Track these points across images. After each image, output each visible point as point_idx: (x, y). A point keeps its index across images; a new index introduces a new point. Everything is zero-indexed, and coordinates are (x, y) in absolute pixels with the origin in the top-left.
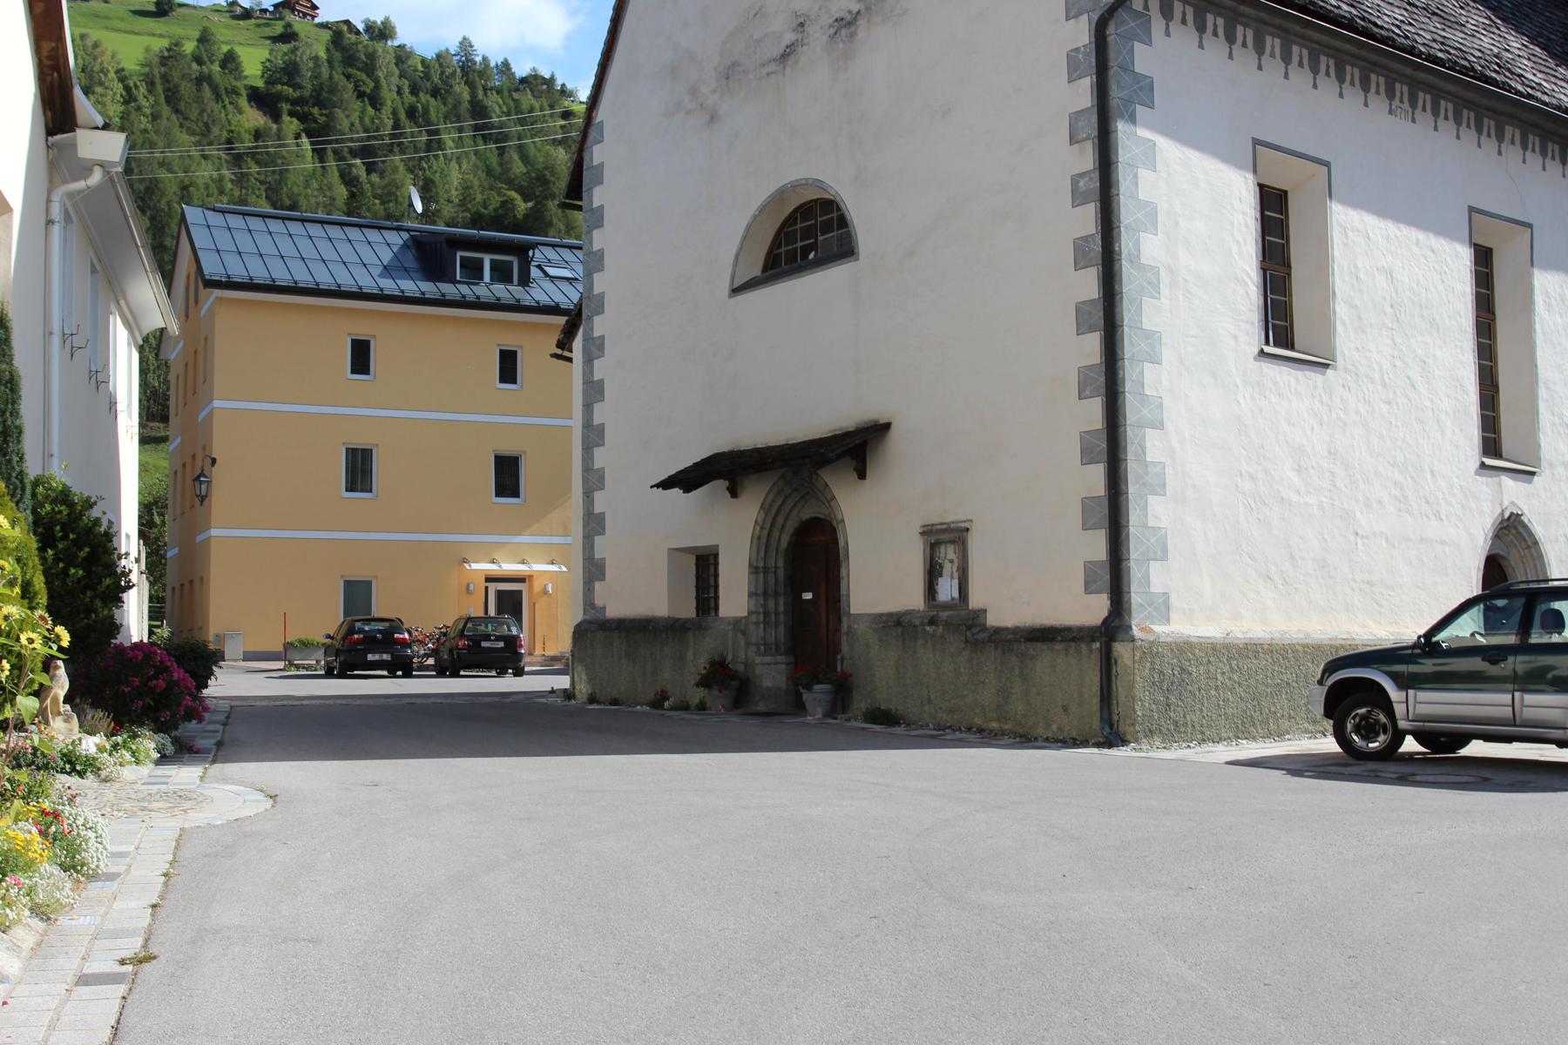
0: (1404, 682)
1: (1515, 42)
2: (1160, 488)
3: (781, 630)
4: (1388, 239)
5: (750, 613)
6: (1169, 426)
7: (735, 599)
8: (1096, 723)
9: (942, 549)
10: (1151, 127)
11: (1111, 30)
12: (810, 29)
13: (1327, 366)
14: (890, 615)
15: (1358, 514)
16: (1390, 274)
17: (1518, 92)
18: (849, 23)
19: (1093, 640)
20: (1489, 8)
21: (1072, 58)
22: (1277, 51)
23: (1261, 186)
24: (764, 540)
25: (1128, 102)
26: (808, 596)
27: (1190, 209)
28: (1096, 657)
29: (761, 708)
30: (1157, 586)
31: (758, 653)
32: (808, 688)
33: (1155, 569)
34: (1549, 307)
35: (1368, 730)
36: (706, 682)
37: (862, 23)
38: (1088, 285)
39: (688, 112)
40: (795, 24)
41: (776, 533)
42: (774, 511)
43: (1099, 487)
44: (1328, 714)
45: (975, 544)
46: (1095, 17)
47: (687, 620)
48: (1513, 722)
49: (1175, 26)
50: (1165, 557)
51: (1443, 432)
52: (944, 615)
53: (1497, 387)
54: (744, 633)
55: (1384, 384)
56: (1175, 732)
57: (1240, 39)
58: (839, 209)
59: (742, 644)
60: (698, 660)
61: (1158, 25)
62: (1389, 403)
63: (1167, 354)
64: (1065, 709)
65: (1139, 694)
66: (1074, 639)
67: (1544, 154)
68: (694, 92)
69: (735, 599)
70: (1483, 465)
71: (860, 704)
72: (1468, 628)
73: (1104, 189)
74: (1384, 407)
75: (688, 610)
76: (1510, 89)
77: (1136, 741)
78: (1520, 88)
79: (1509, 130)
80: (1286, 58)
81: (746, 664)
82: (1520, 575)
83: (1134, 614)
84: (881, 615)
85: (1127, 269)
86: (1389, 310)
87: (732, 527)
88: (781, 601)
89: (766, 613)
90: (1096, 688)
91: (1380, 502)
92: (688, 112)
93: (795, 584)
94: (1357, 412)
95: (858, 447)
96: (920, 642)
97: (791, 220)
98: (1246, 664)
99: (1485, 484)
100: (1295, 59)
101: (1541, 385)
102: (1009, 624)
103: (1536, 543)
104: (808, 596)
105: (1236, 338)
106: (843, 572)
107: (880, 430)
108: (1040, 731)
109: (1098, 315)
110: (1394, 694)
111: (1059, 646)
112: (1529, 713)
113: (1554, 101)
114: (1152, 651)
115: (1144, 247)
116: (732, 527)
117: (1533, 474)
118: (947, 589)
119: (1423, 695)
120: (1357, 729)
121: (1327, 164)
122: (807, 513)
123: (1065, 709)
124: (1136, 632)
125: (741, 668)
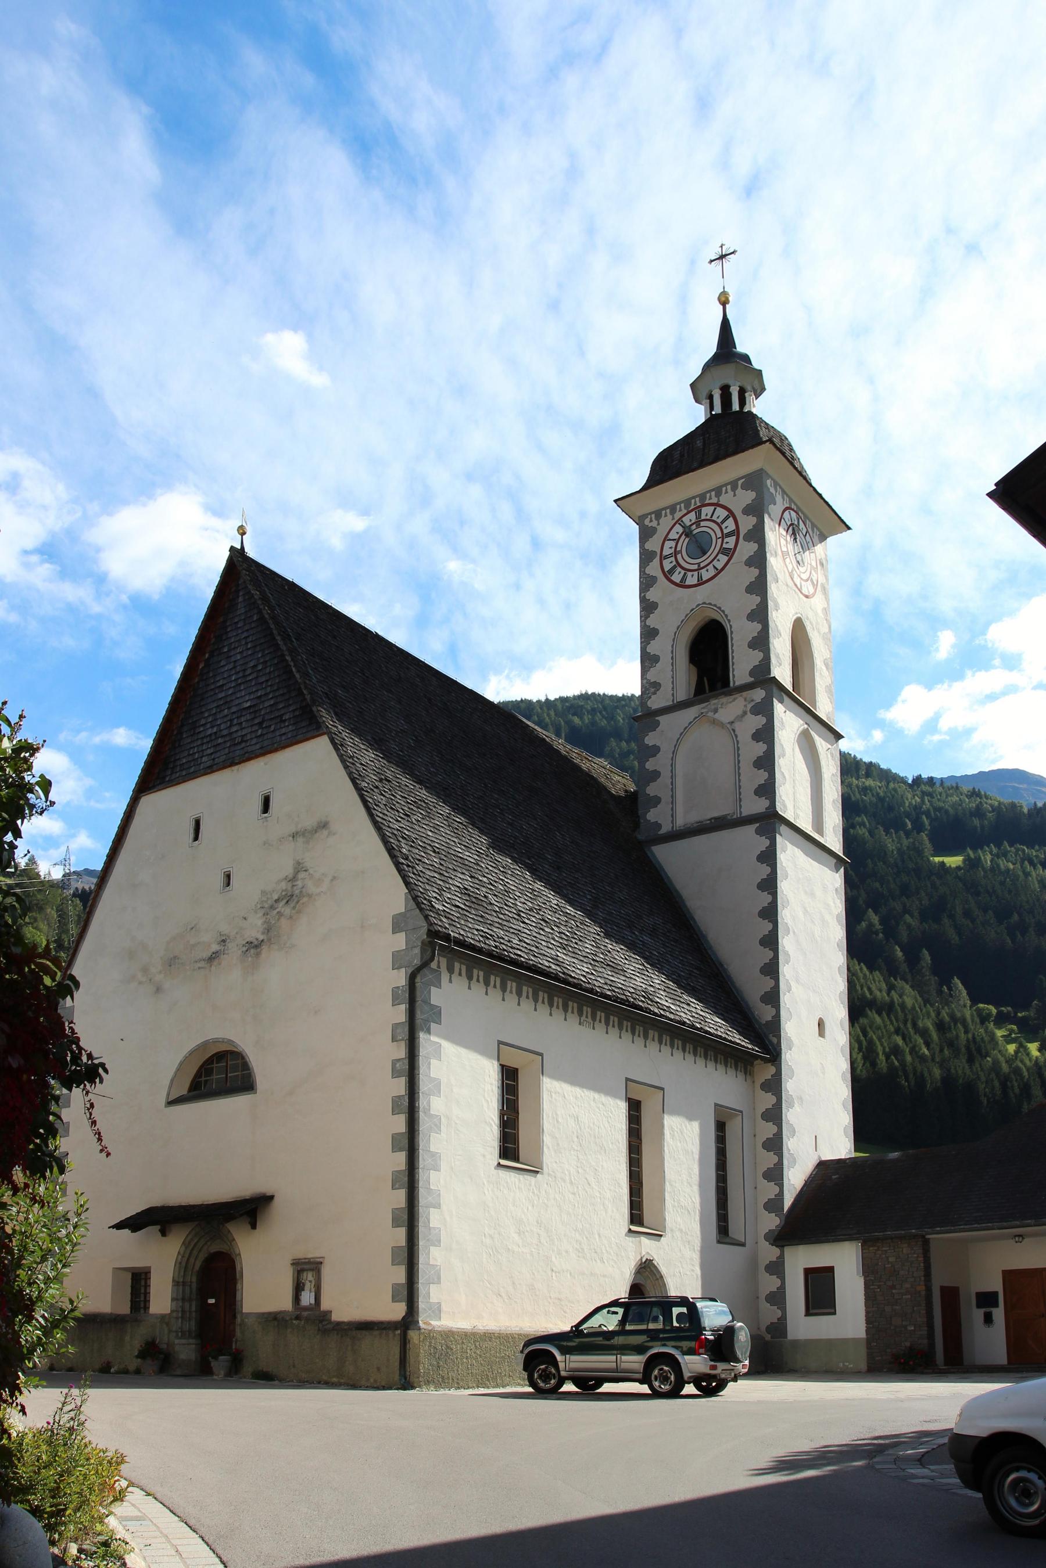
0: (564, 1351)
1: (658, 979)
2: (437, 1243)
3: (193, 1323)
4: (576, 1098)
5: (172, 1311)
6: (444, 1207)
7: (161, 1300)
8: (397, 1377)
9: (305, 1274)
10: (439, 1036)
11: (418, 979)
12: (230, 945)
13: (537, 1172)
14: (270, 1313)
15: (554, 1259)
16: (577, 1119)
17: (655, 1014)
18: (256, 947)
19: (396, 1329)
20: (643, 958)
21: (395, 990)
22: (514, 990)
23: (502, 1066)
24: (184, 1264)
25: (427, 1021)
26: (212, 1301)
27: (461, 1083)
28: (398, 1338)
29: (178, 1372)
30: (434, 1299)
31: (177, 1337)
32: (216, 1358)
33: (433, 1288)
34: (673, 1136)
35: (546, 1377)
36: (143, 1355)
37: (265, 948)
38: (400, 1124)
39: (140, 983)
40: (220, 939)
41: (192, 1260)
42: (192, 1244)
43: (402, 1241)
44: (525, 1369)
45: (326, 1272)
46: (410, 971)
47: (125, 1315)
48: (616, 1370)
49: (455, 977)
50: (439, 1282)
51: (606, 1212)
52: (305, 1314)
53: (641, 1183)
54: (167, 1324)
55: (571, 1183)
56: (442, 1382)
57: (492, 983)
58: (243, 1058)
59: (166, 1332)
60: (134, 1341)
61: (445, 977)
62: (574, 1194)
63: (444, 1166)
64: (378, 1369)
65: (423, 1361)
66: (385, 1329)
67: (672, 1046)
68: (145, 970)
69: (161, 1300)
70: (630, 1230)
71: (248, 1368)
72: (610, 1322)
73: (410, 1069)
74: (571, 1196)
75: (125, 1309)
76: (650, 1012)
77: (420, 1387)
78: (656, 1011)
79: (651, 1033)
80: (519, 994)
81: (168, 1344)
82: (652, 1294)
83: (420, 1314)
84: (263, 1314)
85: (422, 1116)
86: (576, 1139)
87: (162, 1257)
88: (194, 1303)
89: (183, 1312)
90: (397, 1356)
91: (567, 1252)
92: (140, 983)
93: (203, 1293)
94: (555, 1199)
95: (252, 1209)
96: (289, 1330)
97: (210, 1061)
98: (487, 1344)
99: (631, 1241)
100: (524, 994)
101: (667, 1183)
102: (346, 1320)
103: (662, 1277)
104: (212, 1301)
105: (484, 1156)
106: (239, 1286)
107: (266, 1200)
108: (363, 1382)
109: (405, 1142)
110: (559, 1357)
111: (376, 1333)
112: (624, 1366)
113: (677, 1018)
114: (430, 1335)
115: (434, 1104)
116: (162, 1257)
117: (661, 1236)
118: (307, 1298)
119: (574, 1358)
120: (540, 1377)
121: (541, 1055)
122: (215, 1248)
123: (378, 1369)
124: (421, 1324)
125: (165, 1346)
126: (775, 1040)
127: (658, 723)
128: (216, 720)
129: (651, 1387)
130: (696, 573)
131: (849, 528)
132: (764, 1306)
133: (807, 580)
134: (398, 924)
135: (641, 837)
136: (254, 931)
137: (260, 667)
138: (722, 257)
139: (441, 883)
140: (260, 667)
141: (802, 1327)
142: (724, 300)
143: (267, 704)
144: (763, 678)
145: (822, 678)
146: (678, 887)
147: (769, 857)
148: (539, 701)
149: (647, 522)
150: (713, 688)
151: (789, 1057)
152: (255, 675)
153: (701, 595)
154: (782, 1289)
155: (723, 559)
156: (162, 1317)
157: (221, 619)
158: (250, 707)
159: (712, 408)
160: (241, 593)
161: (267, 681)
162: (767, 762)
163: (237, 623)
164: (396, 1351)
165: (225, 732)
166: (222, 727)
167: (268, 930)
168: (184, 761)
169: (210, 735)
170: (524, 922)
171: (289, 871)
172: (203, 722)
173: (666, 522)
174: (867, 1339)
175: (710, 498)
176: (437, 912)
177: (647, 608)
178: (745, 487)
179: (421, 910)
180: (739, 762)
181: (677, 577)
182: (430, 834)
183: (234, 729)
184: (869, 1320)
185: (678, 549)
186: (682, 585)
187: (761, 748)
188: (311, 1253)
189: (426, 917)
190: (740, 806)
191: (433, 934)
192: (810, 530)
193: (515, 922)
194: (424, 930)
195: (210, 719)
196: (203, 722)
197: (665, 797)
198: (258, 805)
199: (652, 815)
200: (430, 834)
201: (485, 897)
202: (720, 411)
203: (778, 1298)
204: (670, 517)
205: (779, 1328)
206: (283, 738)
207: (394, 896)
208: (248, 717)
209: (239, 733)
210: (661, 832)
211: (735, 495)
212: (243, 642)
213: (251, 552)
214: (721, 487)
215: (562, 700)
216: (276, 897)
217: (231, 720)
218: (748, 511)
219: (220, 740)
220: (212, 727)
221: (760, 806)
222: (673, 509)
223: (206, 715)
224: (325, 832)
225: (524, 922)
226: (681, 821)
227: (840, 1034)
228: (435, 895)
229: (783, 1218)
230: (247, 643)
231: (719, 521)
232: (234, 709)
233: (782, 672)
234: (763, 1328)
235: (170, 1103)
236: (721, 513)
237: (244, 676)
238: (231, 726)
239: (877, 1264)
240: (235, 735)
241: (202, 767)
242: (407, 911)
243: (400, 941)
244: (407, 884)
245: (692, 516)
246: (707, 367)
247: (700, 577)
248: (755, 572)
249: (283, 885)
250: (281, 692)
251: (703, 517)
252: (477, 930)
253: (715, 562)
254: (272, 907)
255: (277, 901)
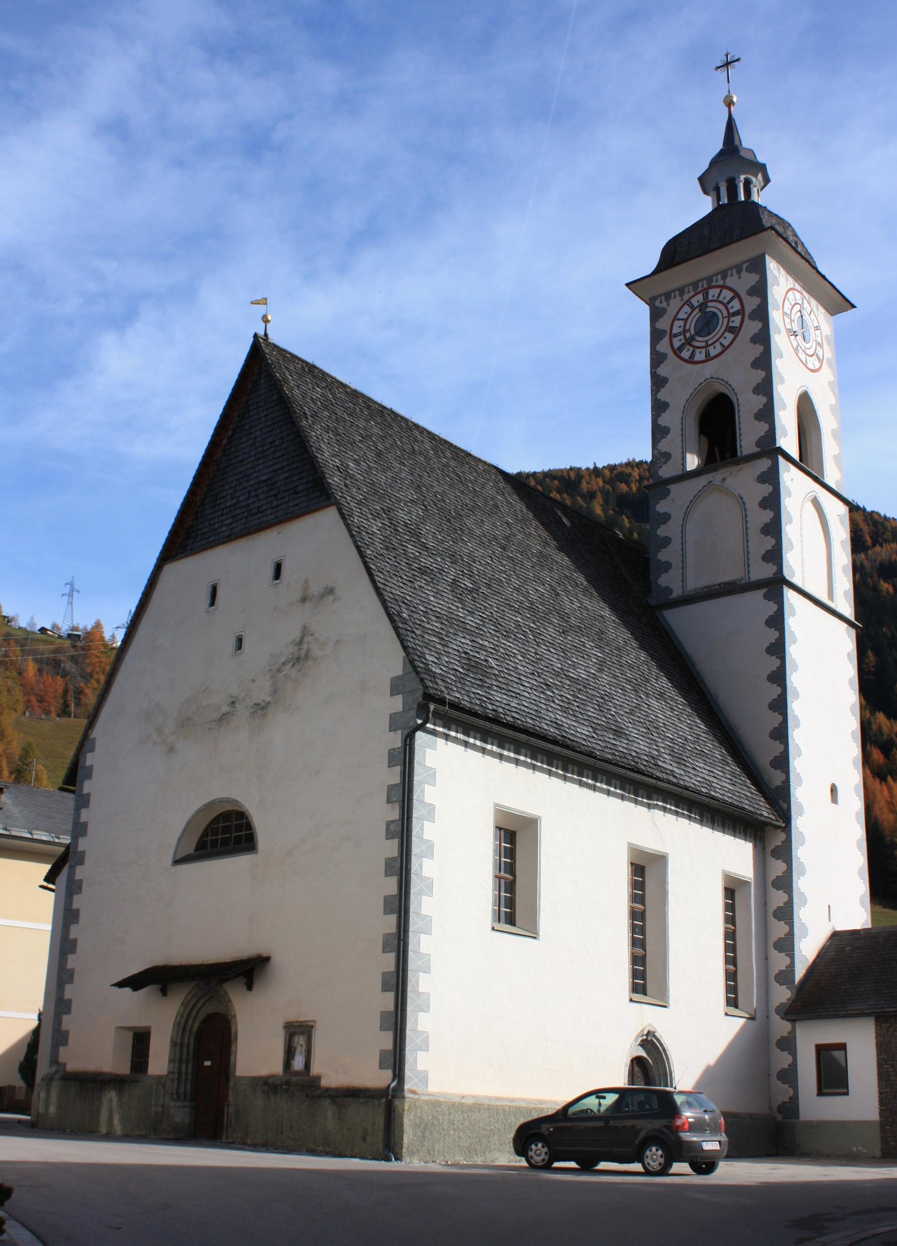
5: (169, 1073)
7: (159, 1062)
12: (238, 705)
17: (658, 778)
18: (263, 708)
30: (420, 1067)
39: (155, 743)
41: (190, 1022)
46: (406, 732)
47: (125, 1076)
52: (294, 1079)
54: (164, 1086)
58: (247, 818)
63: (435, 928)
69: (159, 1062)
75: (124, 1068)
78: (659, 774)
87: (162, 1017)
89: (180, 1074)
92: (155, 743)
95: (250, 970)
97: (216, 820)
106: (233, 1049)
116: (162, 1017)
118: (298, 1063)
126: (785, 806)
127: (669, 492)
128: (236, 492)
129: (644, 1166)
130: (703, 350)
131: (853, 306)
132: (777, 1083)
133: (812, 356)
134: (396, 687)
135: (653, 602)
136: (262, 695)
137: (277, 443)
138: (727, 64)
139: (440, 647)
140: (277, 443)
141: (815, 1107)
142: (729, 103)
143: (282, 477)
144: (770, 449)
145: (830, 448)
146: (689, 651)
147: (777, 621)
148: (588, 469)
149: (657, 303)
150: (723, 458)
151: (800, 823)
152: (272, 450)
153: (709, 370)
154: (794, 1066)
155: (730, 336)
156: (159, 1078)
157: (244, 400)
158: (267, 480)
159: (719, 199)
160: (263, 375)
161: (283, 455)
162: (774, 529)
163: (257, 402)
164: (380, 1120)
165: (243, 504)
166: (241, 498)
167: (275, 692)
168: (205, 530)
169: (230, 506)
170: (523, 685)
171: (296, 635)
172: (224, 494)
173: (676, 302)
174: (881, 1122)
175: (717, 281)
176: (434, 675)
177: (658, 382)
178: (749, 270)
179: (417, 673)
180: (747, 528)
181: (686, 354)
182: (432, 599)
183: (251, 501)
184: (882, 1102)
185: (687, 328)
186: (691, 361)
187: (768, 515)
188: (303, 1016)
189: (422, 680)
190: (749, 572)
191: (428, 697)
192: (815, 309)
193: (515, 685)
194: (420, 693)
195: (230, 491)
196: (224, 494)
197: (676, 561)
198: (270, 572)
199: (664, 580)
200: (432, 599)
201: (486, 661)
202: (726, 201)
203: (789, 1075)
204: (679, 298)
205: (791, 1107)
206: (296, 508)
207: (394, 662)
208: (265, 489)
209: (256, 505)
210: (671, 597)
211: (740, 278)
212: (263, 420)
213: (274, 338)
214: (727, 270)
215: (612, 468)
216: (283, 660)
217: (249, 492)
218: (752, 292)
219: (238, 512)
220: (232, 499)
221: (768, 571)
222: (681, 291)
223: (227, 487)
224: (331, 598)
225: (523, 685)
226: (694, 583)
227: (853, 803)
228: (432, 659)
229: (795, 991)
230: (266, 421)
231: (725, 301)
232: (252, 482)
233: (788, 441)
234: (775, 1108)
235: (177, 862)
236: (727, 294)
237: (263, 451)
238: (248, 498)
239: (890, 1042)
240: (251, 507)
241: (221, 535)
242: (405, 674)
243: (397, 704)
244: (405, 648)
245: (700, 297)
246: (714, 162)
247: (707, 354)
248: (760, 348)
249: (291, 649)
250: (295, 465)
251: (710, 298)
252: (474, 693)
253: (722, 340)
254: (279, 670)
255: (284, 664)
